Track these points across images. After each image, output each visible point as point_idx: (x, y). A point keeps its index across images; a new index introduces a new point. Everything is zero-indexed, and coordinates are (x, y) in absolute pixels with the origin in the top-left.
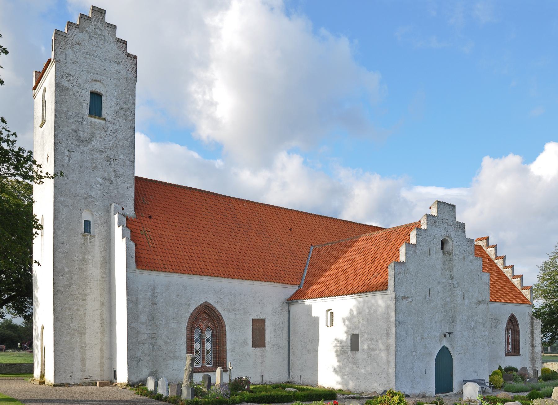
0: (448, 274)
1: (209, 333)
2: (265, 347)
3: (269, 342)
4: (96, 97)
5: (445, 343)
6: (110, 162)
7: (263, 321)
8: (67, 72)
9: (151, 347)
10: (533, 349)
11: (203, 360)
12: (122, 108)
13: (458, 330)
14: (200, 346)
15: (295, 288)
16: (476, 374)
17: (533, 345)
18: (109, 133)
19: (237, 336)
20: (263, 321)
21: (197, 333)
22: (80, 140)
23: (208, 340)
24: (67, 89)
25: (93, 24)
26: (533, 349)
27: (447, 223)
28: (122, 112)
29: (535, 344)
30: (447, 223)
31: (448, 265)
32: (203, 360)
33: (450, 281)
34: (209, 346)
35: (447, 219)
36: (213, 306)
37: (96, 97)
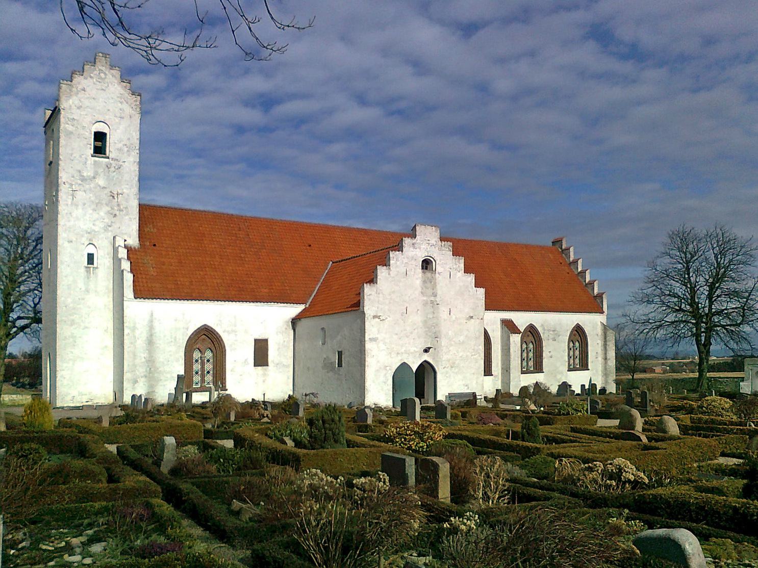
0: (430, 292)
1: (209, 354)
2: (268, 366)
3: (273, 361)
4: (100, 137)
5: (426, 357)
6: (113, 197)
7: (265, 341)
8: (72, 117)
9: (148, 369)
10: (606, 363)
11: (203, 381)
12: (126, 145)
13: (443, 344)
14: (200, 367)
15: (301, 308)
16: (466, 387)
17: (606, 359)
18: (112, 169)
19: (239, 356)
20: (265, 341)
21: (196, 355)
22: (83, 179)
23: (208, 361)
24: (71, 133)
25: (97, 69)
26: (606, 363)
27: (429, 244)
28: (126, 149)
29: (608, 357)
30: (429, 244)
31: (429, 285)
32: (203, 381)
33: (432, 298)
34: (209, 367)
35: (429, 240)
36: (212, 328)
37: (100, 137)
